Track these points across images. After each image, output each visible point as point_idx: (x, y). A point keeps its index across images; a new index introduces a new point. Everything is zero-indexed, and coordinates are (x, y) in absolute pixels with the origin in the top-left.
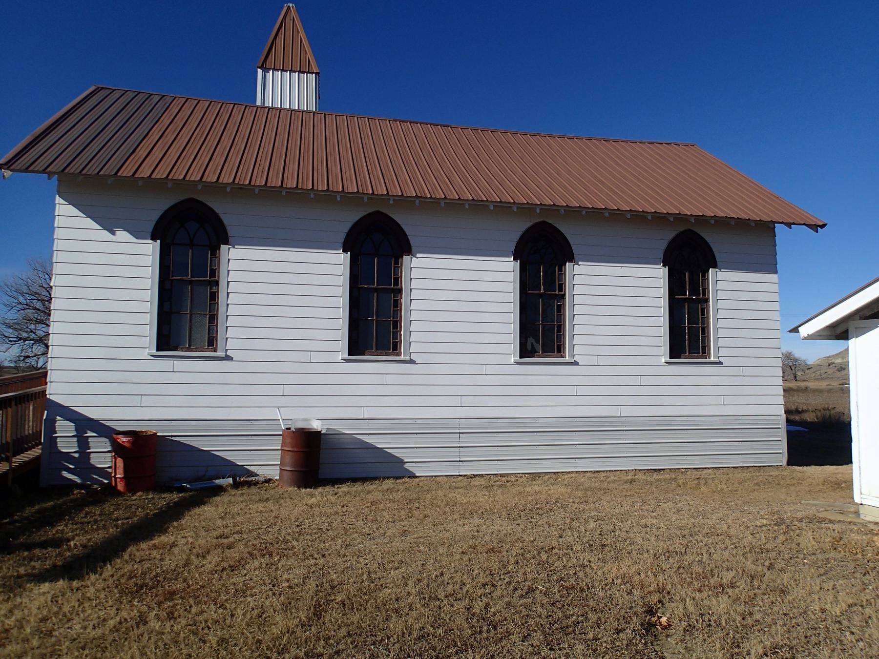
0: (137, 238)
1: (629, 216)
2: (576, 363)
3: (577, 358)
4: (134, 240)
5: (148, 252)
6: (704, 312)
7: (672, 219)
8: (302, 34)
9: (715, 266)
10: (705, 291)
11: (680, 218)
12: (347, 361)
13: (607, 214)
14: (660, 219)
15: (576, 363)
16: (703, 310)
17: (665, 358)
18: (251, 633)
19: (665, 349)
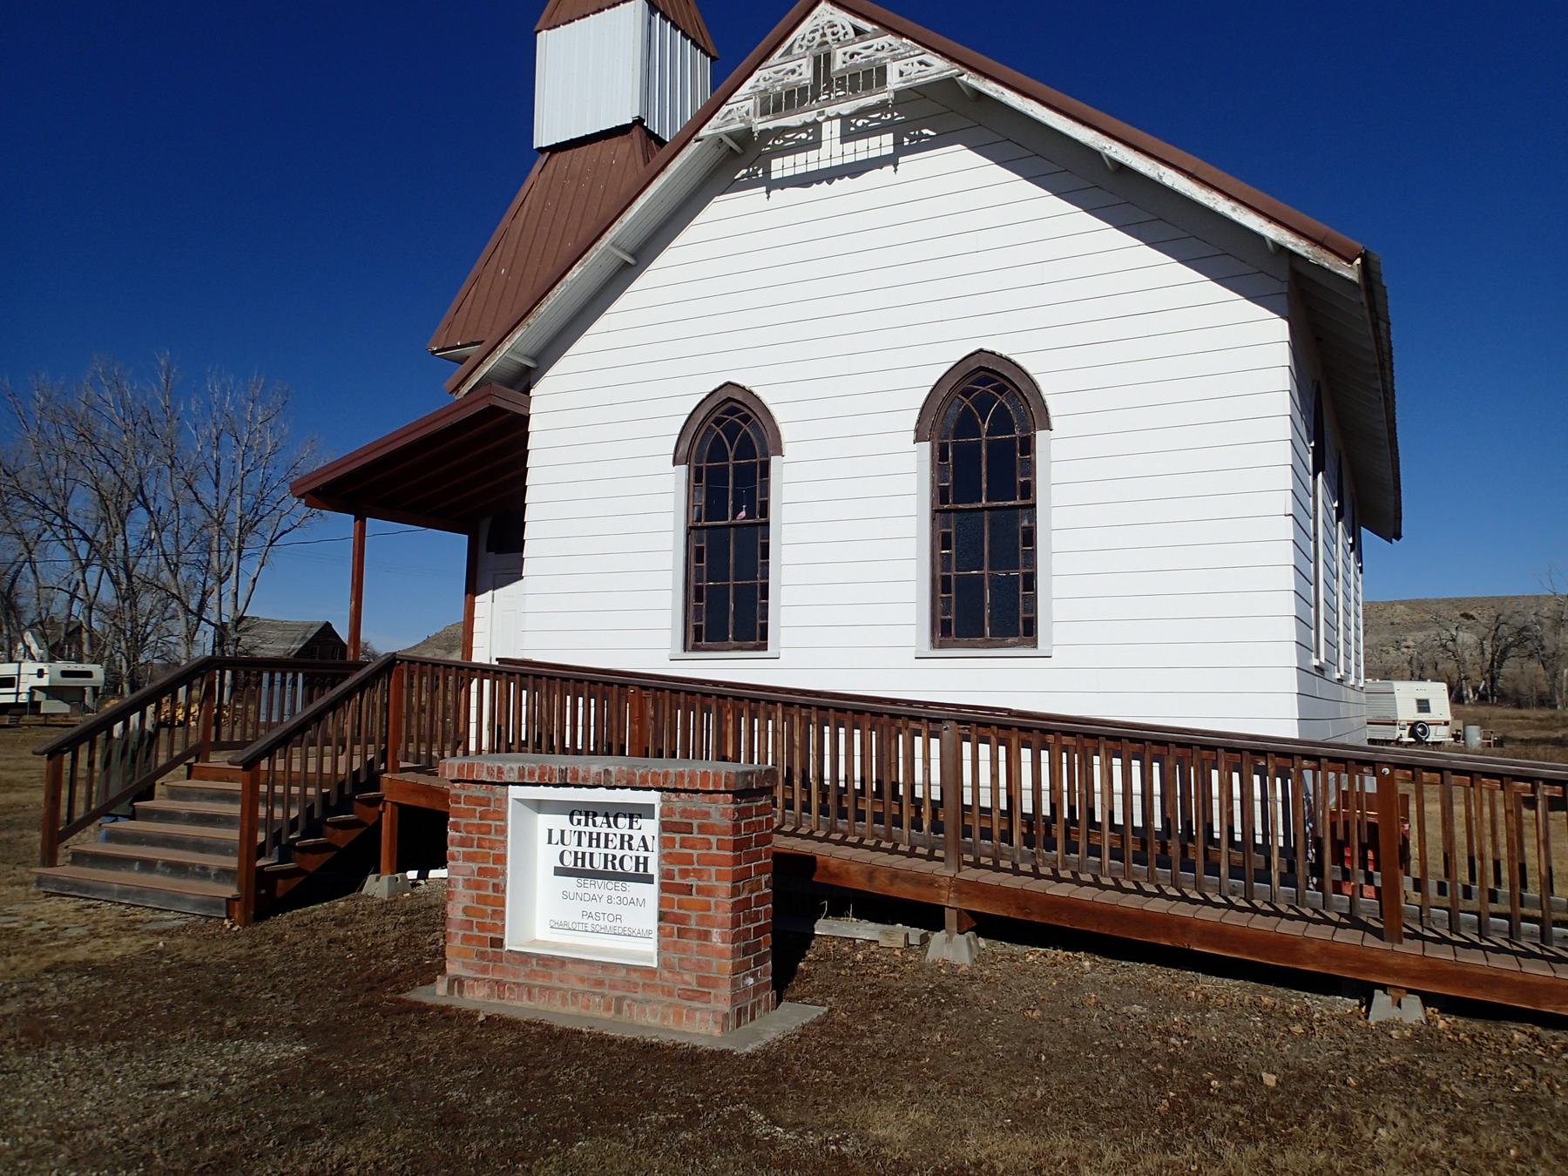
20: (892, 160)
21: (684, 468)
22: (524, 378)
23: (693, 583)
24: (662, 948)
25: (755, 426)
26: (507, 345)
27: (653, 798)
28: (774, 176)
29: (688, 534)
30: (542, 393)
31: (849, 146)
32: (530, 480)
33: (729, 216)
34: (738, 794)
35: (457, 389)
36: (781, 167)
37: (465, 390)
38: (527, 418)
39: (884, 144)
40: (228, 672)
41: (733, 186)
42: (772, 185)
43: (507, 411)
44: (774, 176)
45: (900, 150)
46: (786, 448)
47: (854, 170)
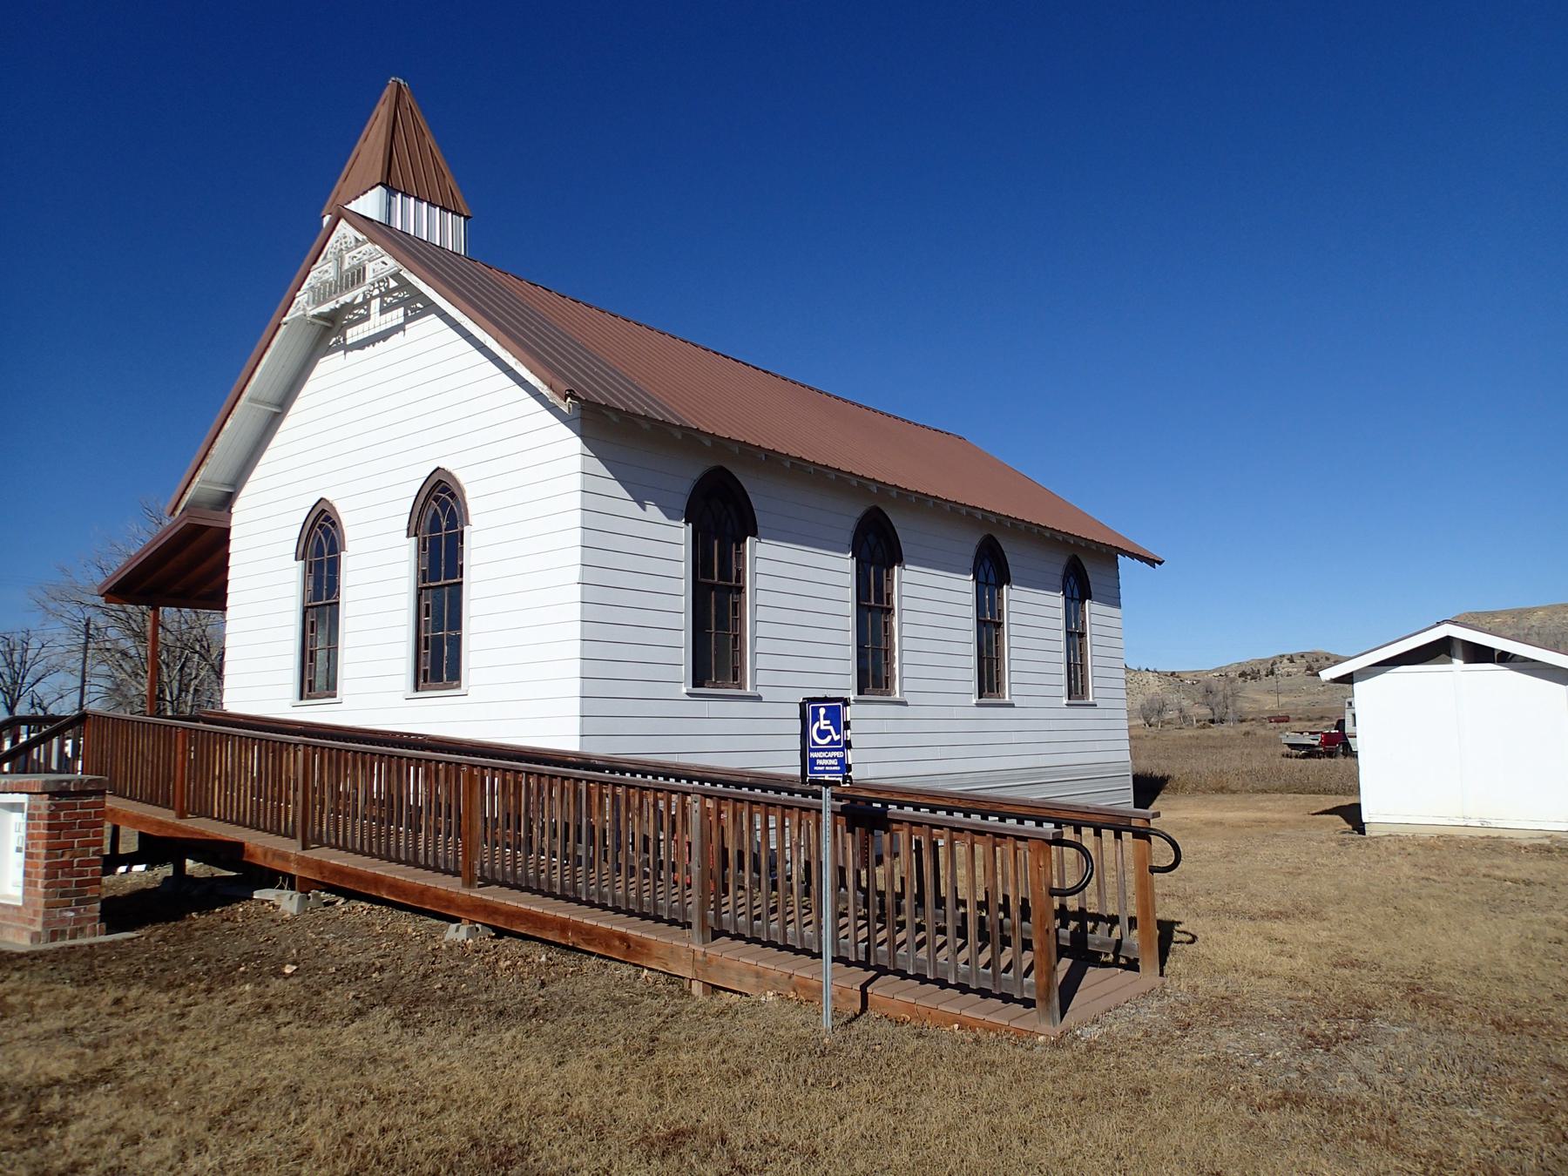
0: (669, 518)
1: (647, 426)
2: (758, 698)
3: (760, 691)
4: (664, 519)
5: (682, 533)
6: (738, 608)
7: (708, 443)
8: (429, 139)
9: (754, 534)
10: (740, 575)
11: (721, 444)
12: (978, 705)
13: (894, 494)
14: (690, 439)
15: (758, 698)
16: (735, 604)
17: (685, 688)
18: (187, 1073)
19: (685, 671)
20: (399, 328)
21: (301, 562)
22: (226, 501)
23: (423, 635)
24: (25, 893)
25: (457, 503)
26: (197, 479)
27: (24, 798)
28: (349, 342)
29: (419, 597)
30: (238, 507)
31: (389, 315)
32: (232, 574)
33: (328, 367)
34: (52, 795)
35: (172, 513)
36: (353, 334)
37: (178, 513)
38: (228, 531)
39: (397, 316)
40: (69, 742)
41: (330, 351)
42: (348, 348)
43: (208, 527)
44: (349, 342)
45: (408, 319)
46: (472, 519)
47: (384, 336)
